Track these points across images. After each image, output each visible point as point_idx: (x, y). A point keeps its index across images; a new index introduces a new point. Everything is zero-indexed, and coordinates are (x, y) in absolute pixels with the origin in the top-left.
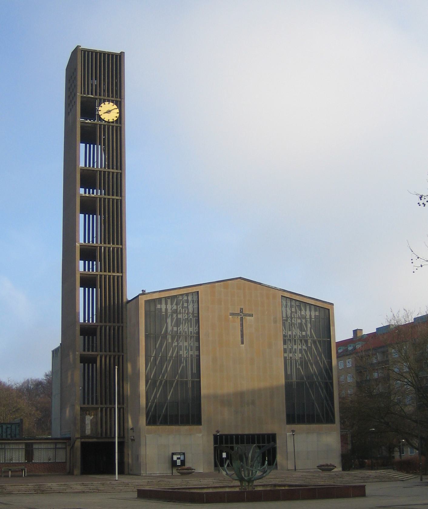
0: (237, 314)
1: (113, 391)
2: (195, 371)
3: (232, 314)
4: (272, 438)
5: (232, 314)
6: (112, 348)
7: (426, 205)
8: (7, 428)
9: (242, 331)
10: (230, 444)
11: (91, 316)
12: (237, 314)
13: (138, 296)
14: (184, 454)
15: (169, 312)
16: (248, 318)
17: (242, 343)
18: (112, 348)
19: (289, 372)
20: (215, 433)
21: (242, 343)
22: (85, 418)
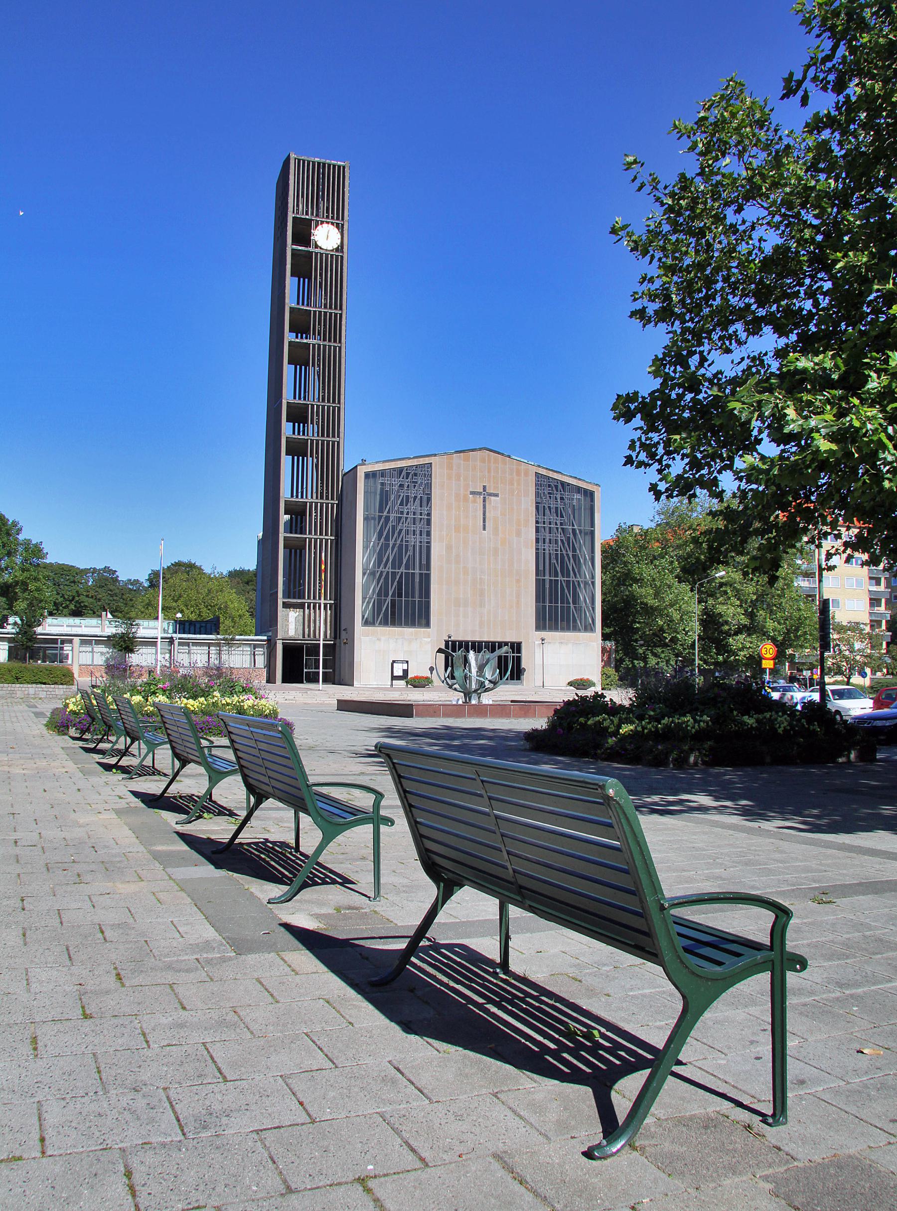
0: (480, 493)
1: (303, 564)
2: (424, 562)
3: (472, 493)
4: (516, 647)
5: (472, 493)
6: (295, 494)
7: (651, 496)
8: (201, 627)
9: (484, 514)
10: (293, 250)
11: (300, 490)
12: (480, 493)
13: (356, 466)
14: (407, 662)
15: (653, 1115)
16: (493, 498)
17: (484, 529)
18: (295, 494)
19: (541, 568)
20: (447, 638)
21: (484, 529)
22: (288, 615)
